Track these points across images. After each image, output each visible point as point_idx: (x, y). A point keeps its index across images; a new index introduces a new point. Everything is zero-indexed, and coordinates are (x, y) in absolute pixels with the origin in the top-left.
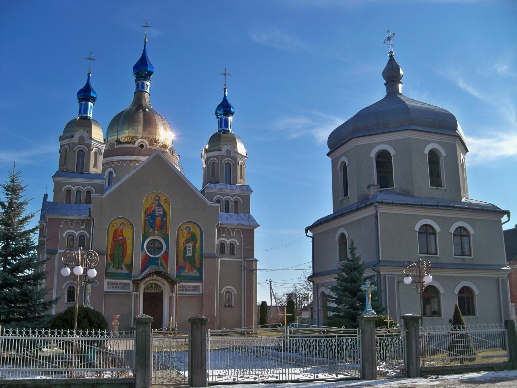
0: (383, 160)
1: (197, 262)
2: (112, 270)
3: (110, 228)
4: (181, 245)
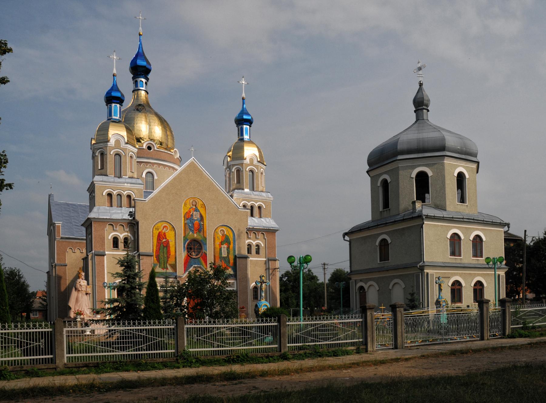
3: (154, 231)
4: (217, 246)
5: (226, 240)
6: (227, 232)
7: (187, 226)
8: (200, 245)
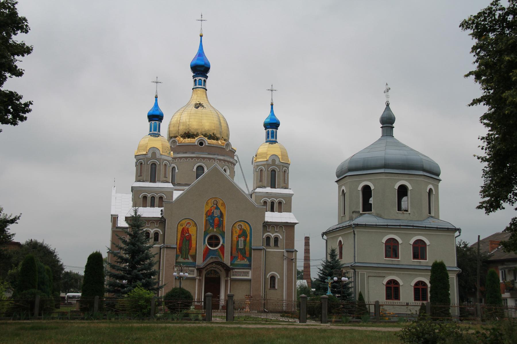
0: (367, 191)
2: (180, 260)
3: (179, 227)
4: (235, 239)
5: (243, 234)
6: (244, 226)
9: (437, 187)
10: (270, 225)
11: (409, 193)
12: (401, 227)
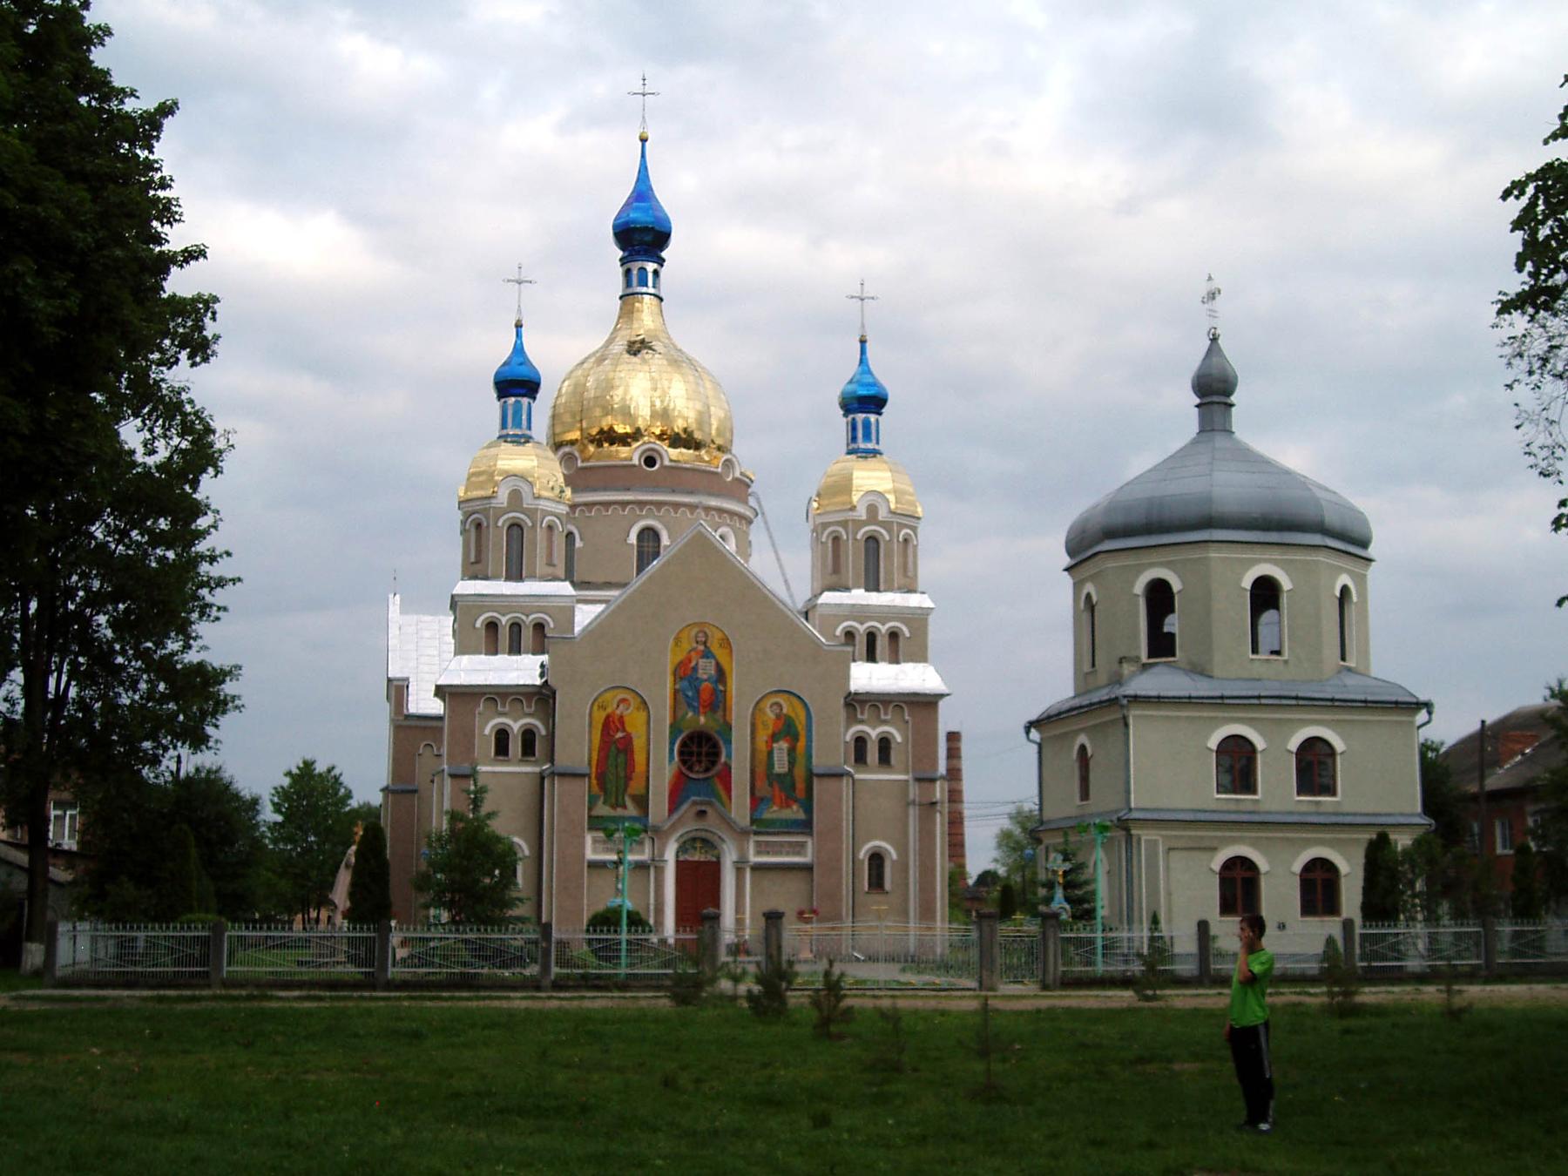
0: (1160, 598)
1: (800, 785)
2: (602, 810)
5: (786, 730)
7: (680, 696)
8: (715, 746)
9: (1361, 580)
10: (865, 702)
11: (1284, 601)
12: (1264, 701)
